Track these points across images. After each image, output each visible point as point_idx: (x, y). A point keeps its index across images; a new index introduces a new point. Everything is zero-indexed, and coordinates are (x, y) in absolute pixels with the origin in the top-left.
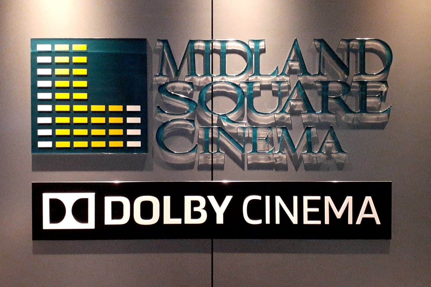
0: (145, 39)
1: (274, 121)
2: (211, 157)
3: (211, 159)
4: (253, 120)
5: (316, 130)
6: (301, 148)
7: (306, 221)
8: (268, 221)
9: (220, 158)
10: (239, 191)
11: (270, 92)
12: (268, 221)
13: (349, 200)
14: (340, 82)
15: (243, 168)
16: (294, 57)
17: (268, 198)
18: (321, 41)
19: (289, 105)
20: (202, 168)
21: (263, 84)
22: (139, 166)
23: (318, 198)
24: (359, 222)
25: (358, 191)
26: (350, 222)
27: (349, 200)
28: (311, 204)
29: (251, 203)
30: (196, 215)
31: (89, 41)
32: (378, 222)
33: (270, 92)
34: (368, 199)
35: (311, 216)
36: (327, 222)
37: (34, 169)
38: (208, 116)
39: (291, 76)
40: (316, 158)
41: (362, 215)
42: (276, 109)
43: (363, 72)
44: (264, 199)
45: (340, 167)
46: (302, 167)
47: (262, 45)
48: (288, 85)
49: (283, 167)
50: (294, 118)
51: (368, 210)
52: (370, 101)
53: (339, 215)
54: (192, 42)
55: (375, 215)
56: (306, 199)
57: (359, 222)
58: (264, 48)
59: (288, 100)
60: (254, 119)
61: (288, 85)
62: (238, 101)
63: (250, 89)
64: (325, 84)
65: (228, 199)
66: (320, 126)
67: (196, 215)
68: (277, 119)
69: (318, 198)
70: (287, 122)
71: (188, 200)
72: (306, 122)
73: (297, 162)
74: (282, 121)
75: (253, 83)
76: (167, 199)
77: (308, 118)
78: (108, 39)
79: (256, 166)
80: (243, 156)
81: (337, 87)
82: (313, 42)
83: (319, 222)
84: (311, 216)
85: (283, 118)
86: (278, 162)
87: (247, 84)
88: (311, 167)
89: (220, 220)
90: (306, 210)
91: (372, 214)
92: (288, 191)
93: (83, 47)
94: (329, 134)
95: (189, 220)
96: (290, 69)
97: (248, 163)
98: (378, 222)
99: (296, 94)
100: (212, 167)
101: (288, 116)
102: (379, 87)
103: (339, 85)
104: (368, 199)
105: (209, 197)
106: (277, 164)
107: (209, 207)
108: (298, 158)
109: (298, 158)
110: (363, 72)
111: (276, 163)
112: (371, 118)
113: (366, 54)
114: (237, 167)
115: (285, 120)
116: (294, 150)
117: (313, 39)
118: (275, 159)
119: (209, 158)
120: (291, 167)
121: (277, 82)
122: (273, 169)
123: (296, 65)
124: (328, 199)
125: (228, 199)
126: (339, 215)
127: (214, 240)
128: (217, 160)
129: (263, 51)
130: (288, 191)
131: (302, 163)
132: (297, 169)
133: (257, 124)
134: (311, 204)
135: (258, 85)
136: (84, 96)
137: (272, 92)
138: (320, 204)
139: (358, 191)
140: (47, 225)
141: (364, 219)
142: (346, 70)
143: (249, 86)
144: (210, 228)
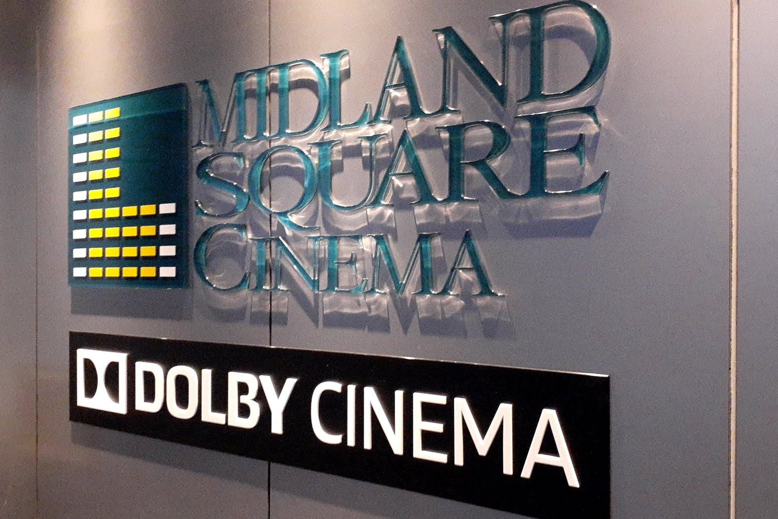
0: (181, 86)
1: (366, 224)
2: (269, 297)
3: (269, 302)
4: (332, 223)
5: (442, 241)
6: (413, 282)
7: (419, 453)
8: (351, 442)
9: (283, 302)
10: (307, 367)
11: (359, 162)
12: (351, 442)
13: (505, 412)
14: (488, 125)
15: (316, 321)
16: (399, 80)
17: (351, 389)
18: (448, 32)
19: (391, 187)
20: (256, 318)
21: (348, 144)
22: (176, 313)
23: (441, 400)
24: (526, 473)
25: (529, 391)
26: (508, 468)
27: (505, 412)
28: (430, 412)
29: (326, 395)
30: (244, 411)
31: (121, 102)
32: (573, 480)
33: (359, 162)
34: (549, 416)
35: (430, 441)
36: (459, 460)
37: (74, 311)
38: (265, 218)
39: (394, 121)
40: (442, 305)
41: (535, 456)
42: (345, 206)
43: (535, 93)
44: (345, 390)
45: (491, 329)
46: (414, 326)
47: (343, 63)
48: (389, 143)
49: (378, 324)
50: (403, 215)
51: (549, 446)
52: (558, 165)
53: (483, 446)
54: (239, 76)
55: (564, 460)
56: (419, 398)
57: (526, 473)
58: (348, 67)
59: (387, 177)
60: (334, 222)
61: (389, 143)
62: (306, 183)
63: (323, 158)
64: (456, 131)
65: (290, 383)
66: (446, 231)
67: (244, 411)
68: (372, 220)
69: (441, 400)
70: (389, 225)
71: (234, 378)
72: (422, 225)
73: (405, 311)
74: (379, 223)
75: (330, 143)
76: (207, 373)
77: (429, 213)
78: (160, 89)
79: (338, 321)
80: (316, 296)
81: (484, 137)
82: (492, 27)
83: (442, 458)
84: (430, 441)
85: (381, 216)
86: (373, 313)
87: (318, 147)
88: (435, 326)
89: (277, 427)
90: (420, 425)
91: (559, 456)
92: (390, 375)
93: (113, 113)
94: (466, 251)
95: (235, 420)
96: (393, 105)
97: (325, 312)
98: (573, 480)
99: (403, 162)
100: (270, 319)
101: (389, 212)
102: (579, 125)
103: (487, 131)
104: (549, 416)
105: (262, 377)
106: (371, 317)
107: (261, 397)
108: (408, 305)
109: (408, 305)
110: (535, 93)
111: (370, 315)
112: (562, 208)
113: (547, 45)
114: (307, 320)
115: (386, 219)
116: (399, 288)
117: (431, 29)
118: (369, 305)
119: (267, 300)
120: (395, 323)
121: (369, 139)
122: (364, 329)
123: (401, 96)
124: (461, 405)
125: (290, 383)
126: (483, 446)
127: (272, 465)
128: (278, 306)
129: (347, 74)
130: (390, 375)
131: (415, 317)
132: (405, 329)
133: (339, 231)
134: (430, 412)
135: (340, 147)
136: (113, 192)
137: (363, 160)
138: (444, 414)
139: (529, 391)
140: (83, 401)
141: (538, 467)
142: (500, 94)
143: (323, 151)
144: (255, 443)
